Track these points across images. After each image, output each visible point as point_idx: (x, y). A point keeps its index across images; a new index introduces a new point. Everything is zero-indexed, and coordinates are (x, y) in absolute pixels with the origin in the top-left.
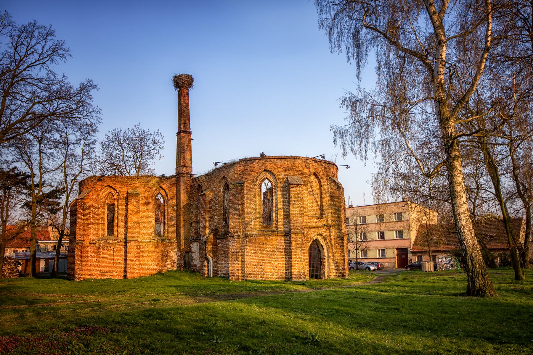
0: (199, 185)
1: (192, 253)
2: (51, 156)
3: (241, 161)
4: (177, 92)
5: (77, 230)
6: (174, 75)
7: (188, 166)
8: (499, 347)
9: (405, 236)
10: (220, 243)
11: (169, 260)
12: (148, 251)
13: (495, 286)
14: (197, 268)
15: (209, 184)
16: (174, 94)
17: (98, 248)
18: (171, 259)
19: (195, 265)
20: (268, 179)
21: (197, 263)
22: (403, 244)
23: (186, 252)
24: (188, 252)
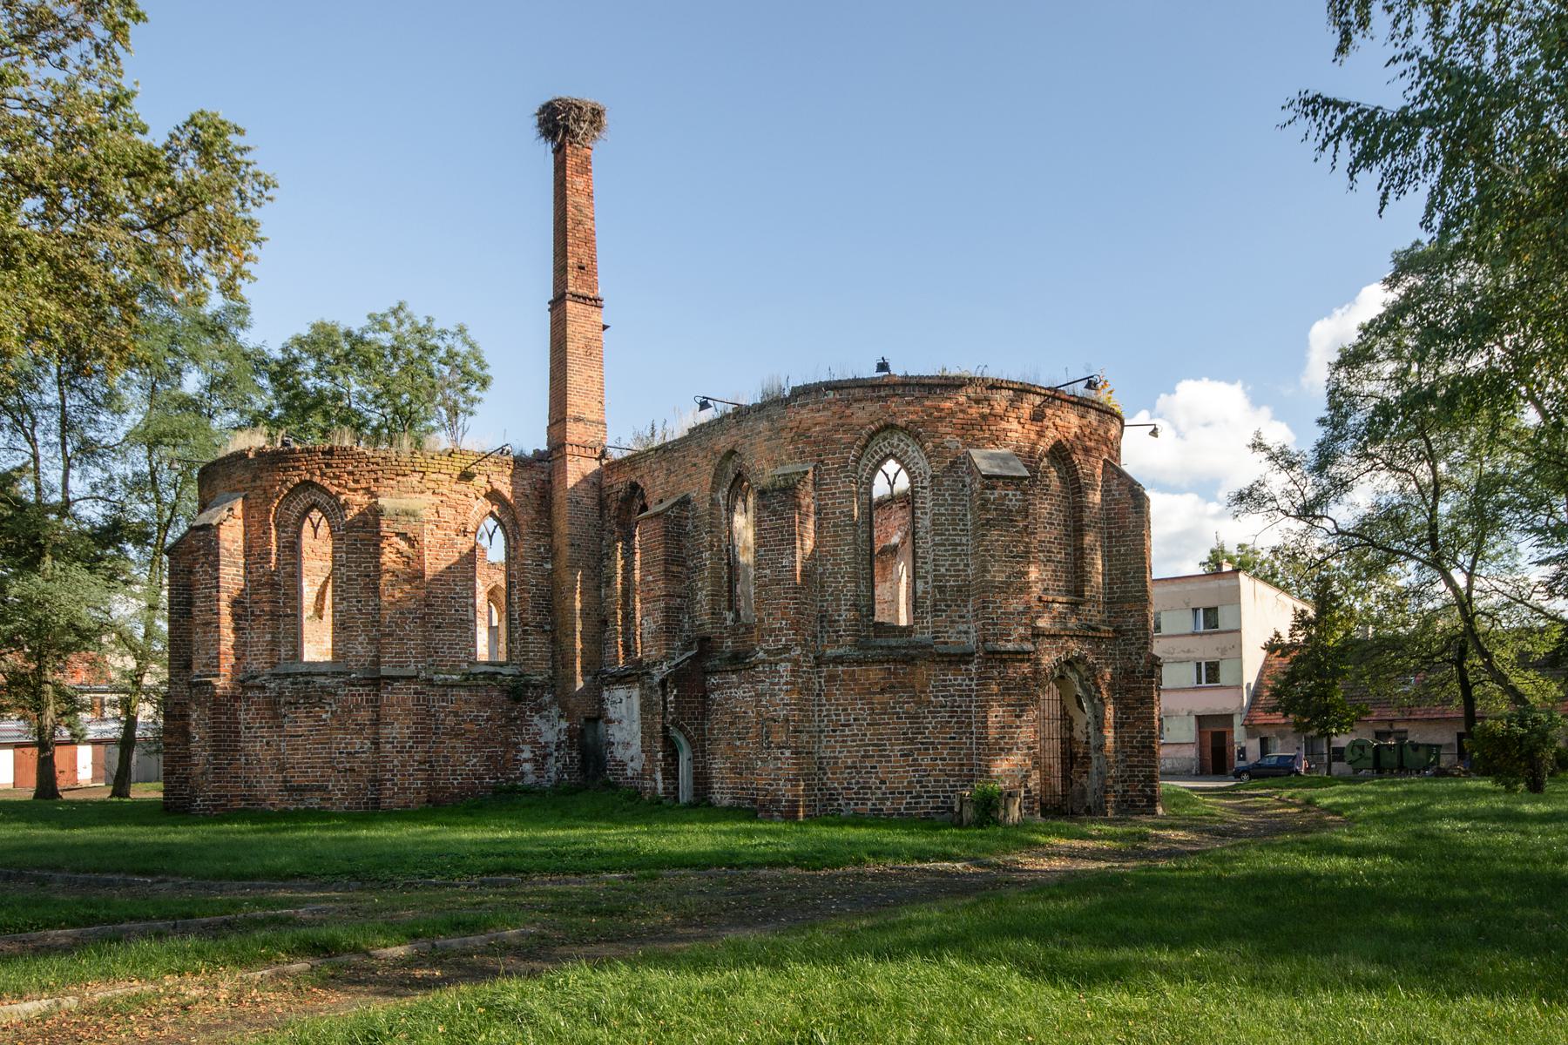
0: (634, 487)
1: (610, 721)
2: (111, 401)
3: (798, 392)
4: (549, 147)
5: (196, 637)
6: (535, 132)
7: (594, 417)
8: (948, 848)
9: (1225, 677)
10: (718, 687)
11: (527, 748)
12: (456, 714)
13: (788, 753)
14: (629, 773)
15: (673, 479)
16: (544, 152)
17: (273, 704)
18: (536, 742)
19: (622, 765)
20: (899, 460)
21: (626, 758)
22: (1213, 701)
23: (587, 720)
24: (595, 720)
